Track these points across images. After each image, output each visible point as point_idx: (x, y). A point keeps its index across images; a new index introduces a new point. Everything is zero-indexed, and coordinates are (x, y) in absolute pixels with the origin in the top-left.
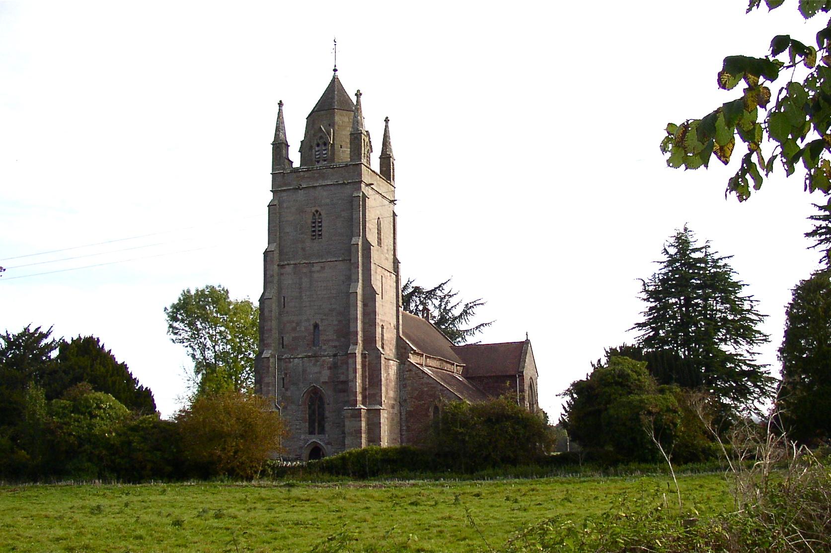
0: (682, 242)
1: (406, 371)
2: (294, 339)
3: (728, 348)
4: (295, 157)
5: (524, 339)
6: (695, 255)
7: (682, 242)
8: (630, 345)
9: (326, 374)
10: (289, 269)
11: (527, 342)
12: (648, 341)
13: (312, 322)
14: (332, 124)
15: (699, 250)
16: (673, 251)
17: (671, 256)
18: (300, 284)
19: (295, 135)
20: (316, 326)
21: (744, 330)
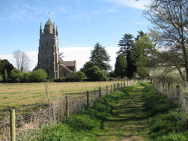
0: (97, 44)
1: (60, 66)
3: (104, 62)
4: (43, 31)
6: (100, 47)
7: (97, 44)
8: (117, 57)
9: (49, 66)
10: (43, 50)
14: (49, 27)
16: (96, 46)
19: (43, 28)
20: (47, 59)
21: (107, 59)
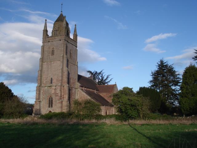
2: (46, 82)
5: (115, 84)
11: (116, 85)
12: (152, 86)
13: (51, 77)
15: (165, 63)
17: (159, 64)
18: (48, 67)
